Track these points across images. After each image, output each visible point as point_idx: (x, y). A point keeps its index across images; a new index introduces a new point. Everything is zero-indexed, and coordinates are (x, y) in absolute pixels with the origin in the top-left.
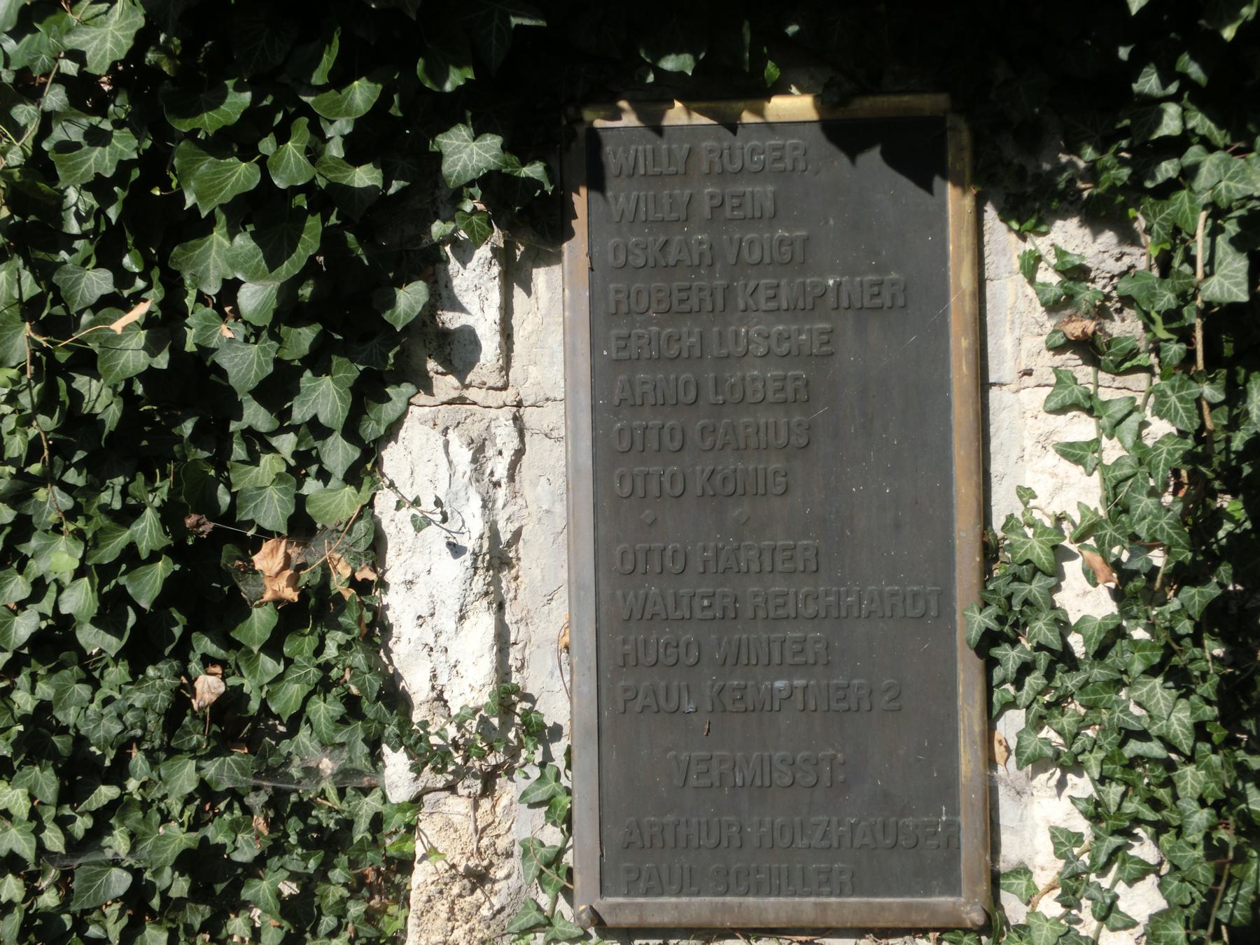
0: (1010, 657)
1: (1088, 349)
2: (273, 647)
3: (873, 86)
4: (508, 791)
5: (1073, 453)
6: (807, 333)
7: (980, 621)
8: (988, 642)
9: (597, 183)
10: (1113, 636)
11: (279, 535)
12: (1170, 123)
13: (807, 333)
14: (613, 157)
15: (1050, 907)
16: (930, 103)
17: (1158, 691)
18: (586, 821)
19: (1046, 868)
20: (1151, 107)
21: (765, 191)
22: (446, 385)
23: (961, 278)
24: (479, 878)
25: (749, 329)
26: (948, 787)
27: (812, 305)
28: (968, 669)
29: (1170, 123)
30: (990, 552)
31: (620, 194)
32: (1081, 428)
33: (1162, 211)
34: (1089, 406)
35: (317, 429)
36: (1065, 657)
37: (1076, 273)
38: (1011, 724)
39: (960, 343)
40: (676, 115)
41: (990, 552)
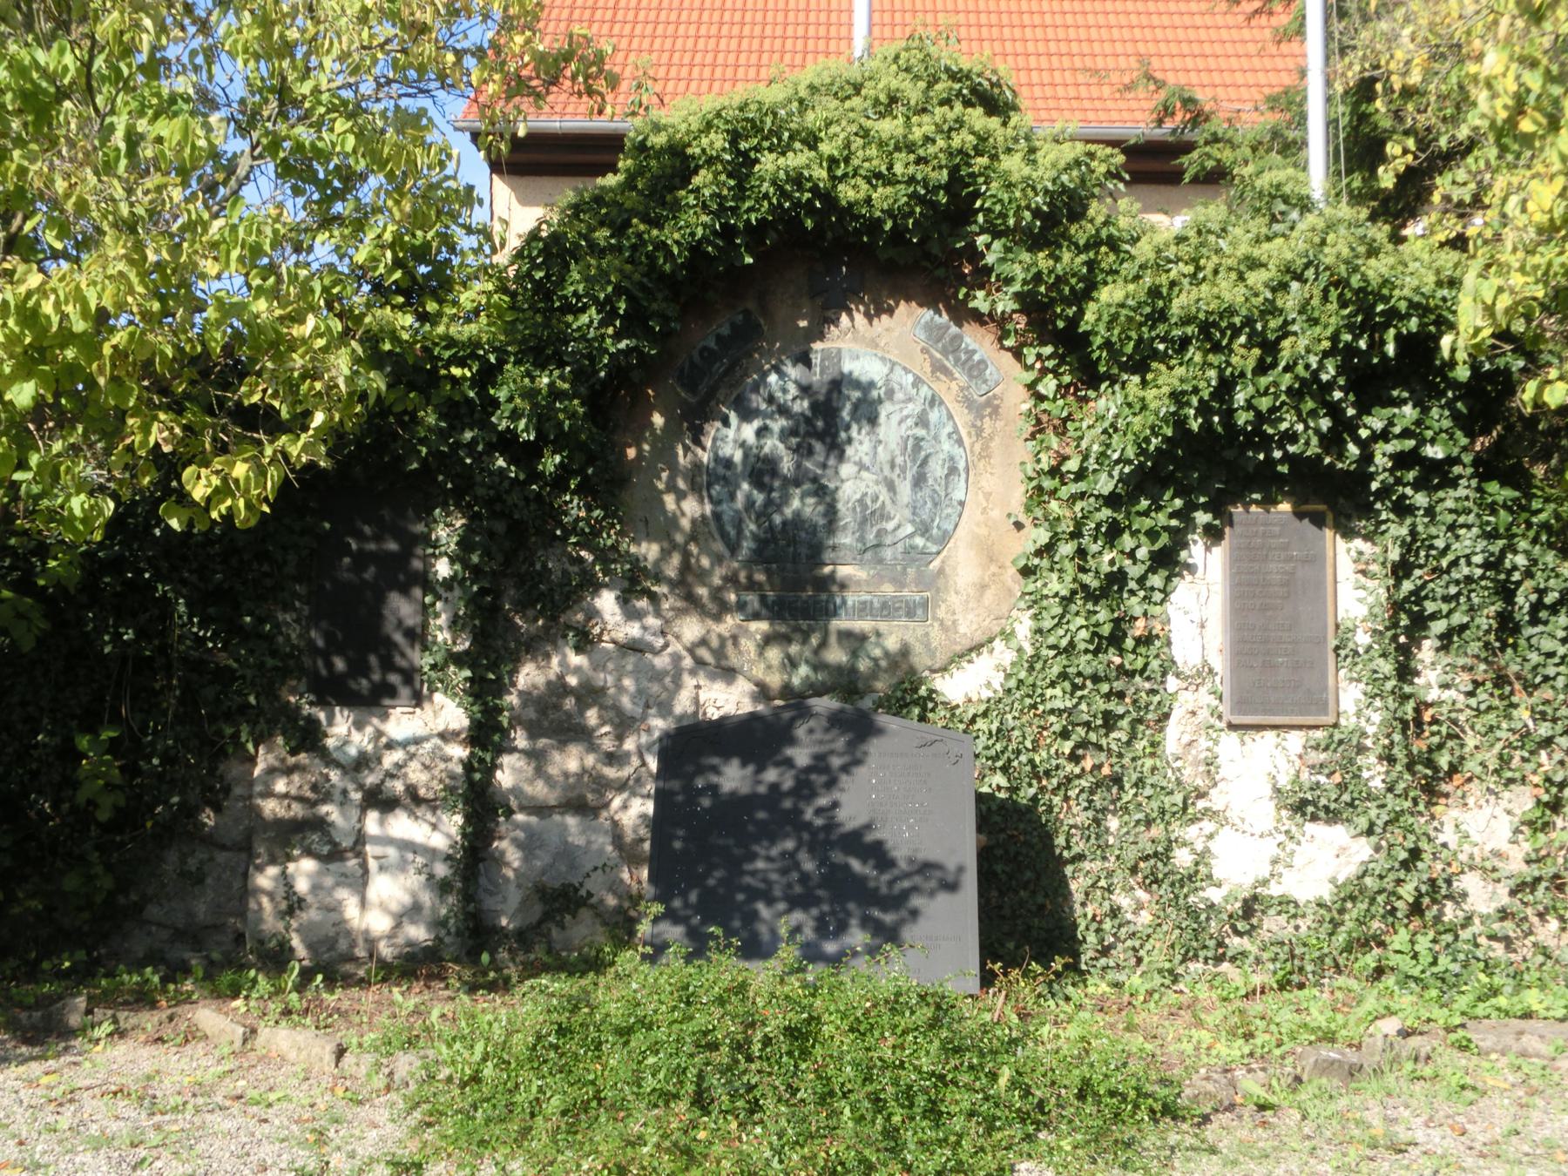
0: (1343, 653)
1: (1364, 572)
2: (1134, 652)
3: (1306, 502)
4: (1203, 690)
5: (1360, 600)
6: (1288, 567)
7: (1335, 642)
8: (1337, 648)
9: (1231, 524)
10: (1369, 649)
11: (284, 873)
12: (1384, 516)
13: (1288, 567)
14: (1236, 519)
15: (1353, 719)
16: (1322, 507)
17: (1381, 661)
18: (1226, 696)
19: (1352, 710)
20: (1379, 512)
21: (1277, 529)
22: (1188, 578)
23: (1330, 553)
24: (1194, 713)
25: (1272, 566)
26: (1325, 688)
27: (1290, 559)
28: (1331, 656)
29: (1384, 516)
30: (1337, 626)
31: (1238, 529)
32: (1362, 593)
33: (519, 886)
34: (1364, 588)
35: (1152, 589)
36: (1356, 653)
37: (1361, 553)
38: (1342, 673)
39: (1329, 571)
40: (1253, 508)
41: (1337, 626)
